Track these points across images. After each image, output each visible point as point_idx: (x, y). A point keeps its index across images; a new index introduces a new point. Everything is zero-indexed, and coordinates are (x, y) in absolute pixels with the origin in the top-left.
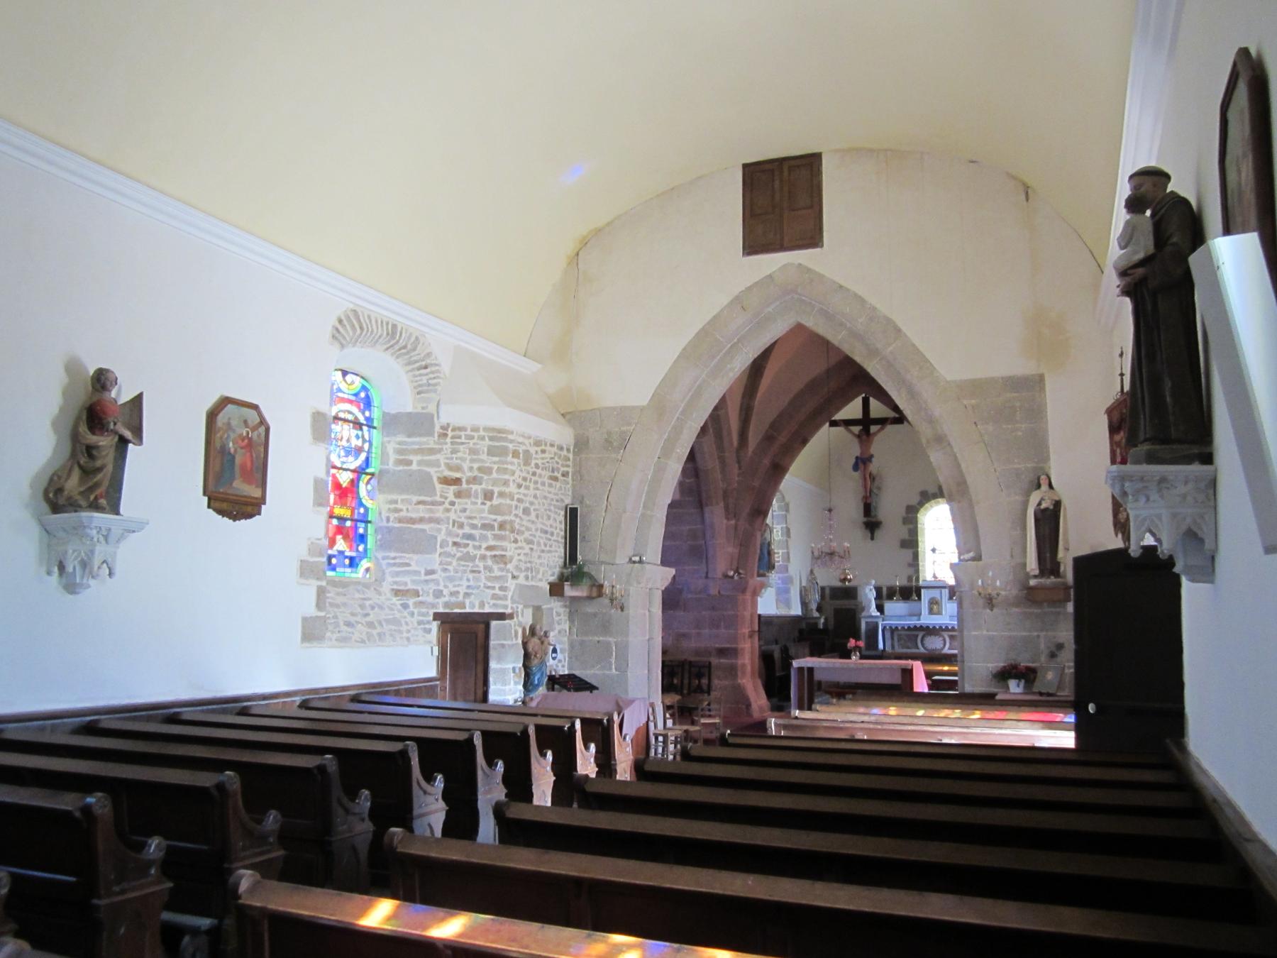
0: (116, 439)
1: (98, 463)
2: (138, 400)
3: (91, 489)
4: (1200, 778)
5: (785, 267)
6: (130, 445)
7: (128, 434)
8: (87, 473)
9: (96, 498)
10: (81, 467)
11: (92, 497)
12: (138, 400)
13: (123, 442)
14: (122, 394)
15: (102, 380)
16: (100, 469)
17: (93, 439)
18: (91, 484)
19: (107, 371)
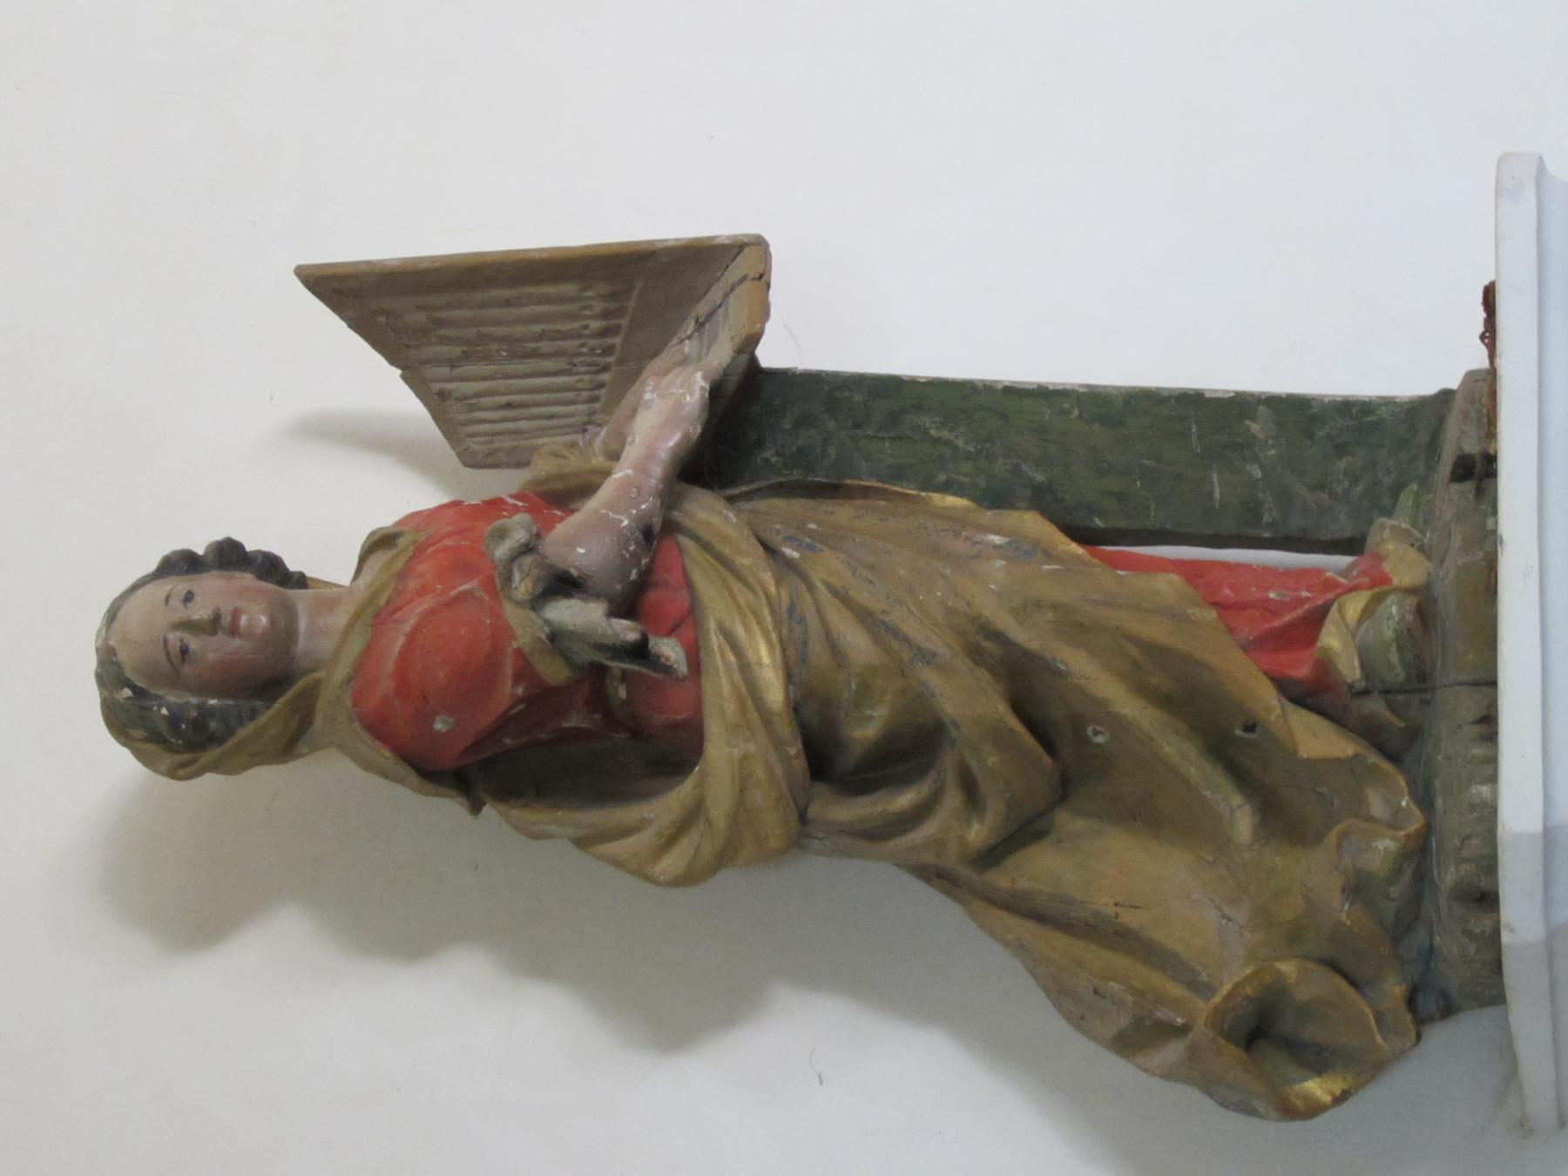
0: (706, 511)
1: (968, 700)
2: (379, 301)
3: (1232, 744)
4: (538, 256)
5: (1013, 731)
6: (770, 355)
7: (666, 408)
8: (1062, 758)
9: (1317, 695)
10: (1024, 831)
11: (1315, 739)
12: (379, 301)
13: (760, 431)
14: (330, 476)
15: (211, 684)
16: (1025, 684)
17: (737, 755)
18: (1178, 750)
19: (110, 673)
